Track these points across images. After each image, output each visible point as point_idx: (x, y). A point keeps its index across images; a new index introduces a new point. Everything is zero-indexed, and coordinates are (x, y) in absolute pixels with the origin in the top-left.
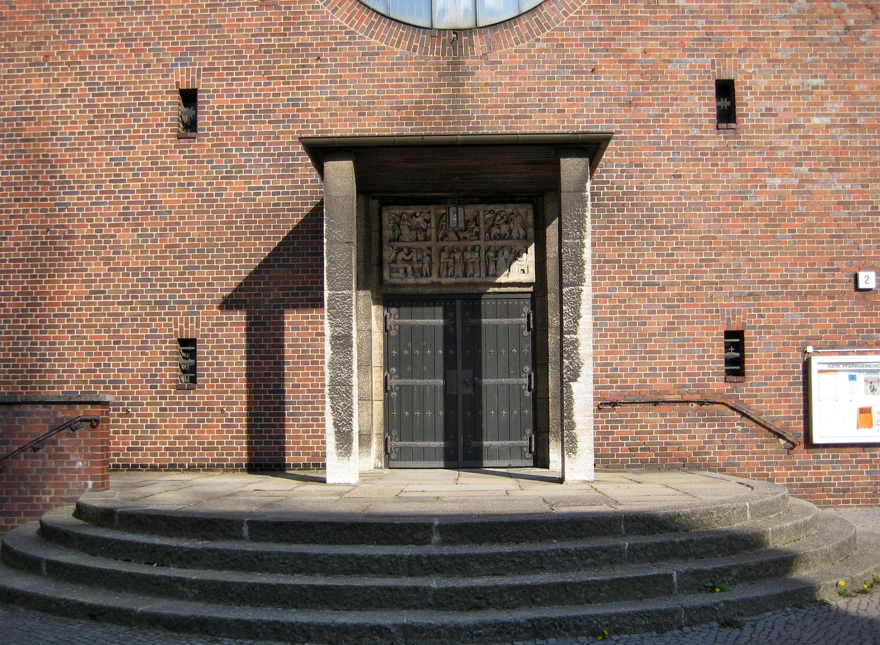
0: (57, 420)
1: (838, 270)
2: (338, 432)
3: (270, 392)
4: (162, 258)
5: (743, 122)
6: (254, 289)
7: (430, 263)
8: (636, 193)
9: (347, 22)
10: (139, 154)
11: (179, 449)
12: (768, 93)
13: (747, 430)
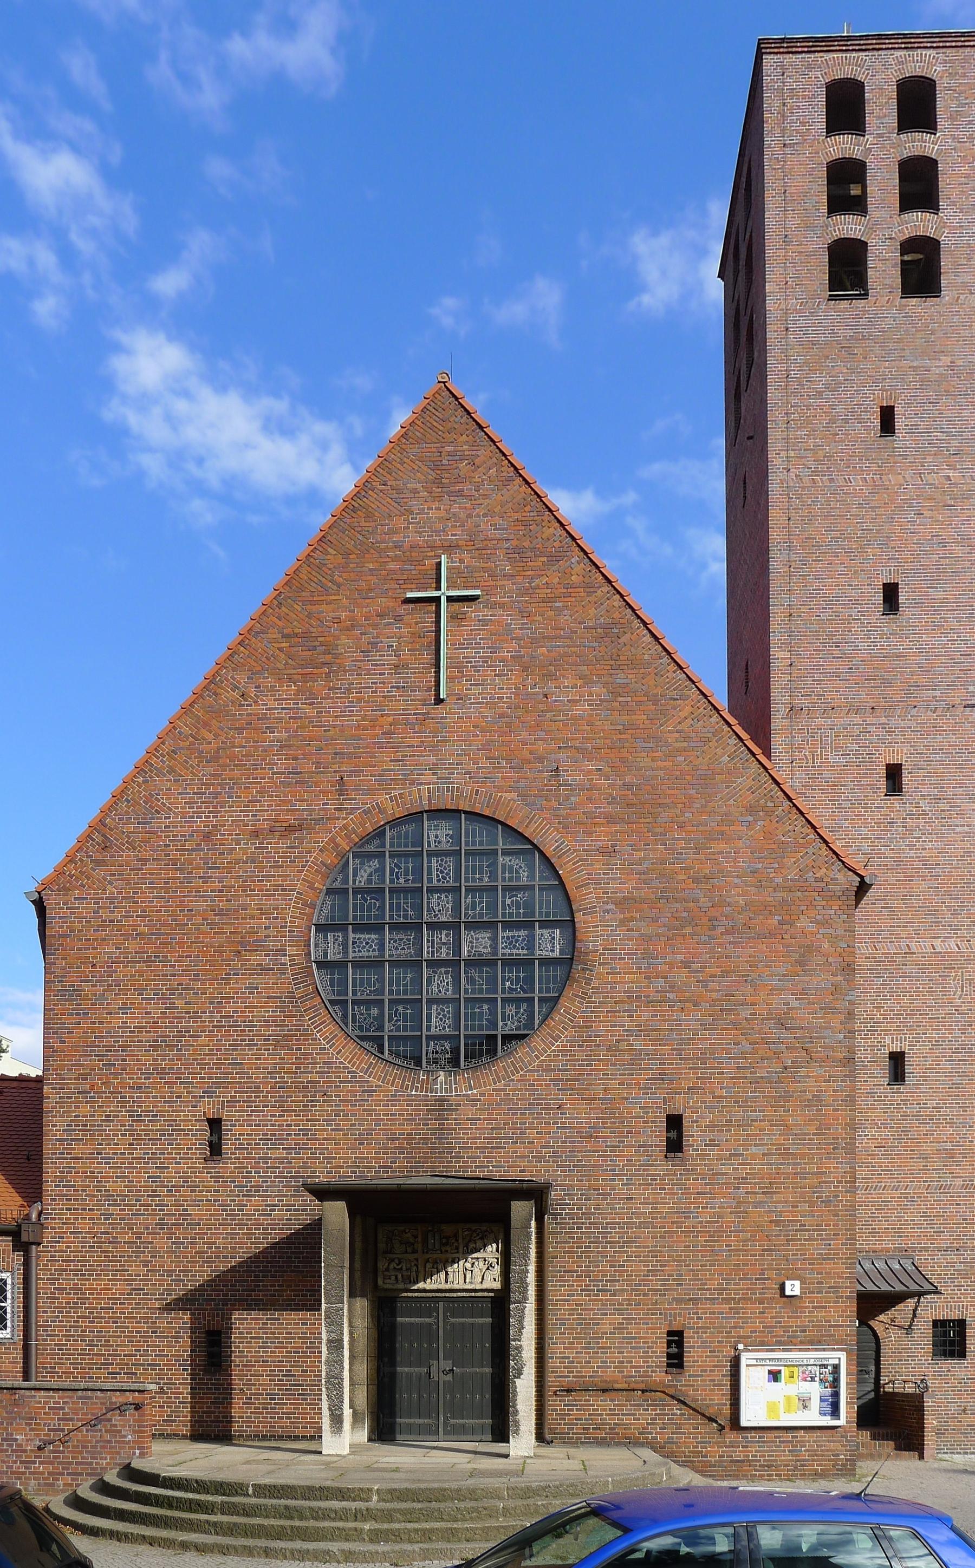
0: (111, 1403)
1: (768, 1279)
2: (332, 1415)
3: (283, 1376)
4: (193, 1262)
5: (689, 1152)
6: (270, 1290)
7: (417, 1272)
8: (594, 1214)
9: (349, 1063)
10: (172, 1174)
11: (206, 1421)
12: (712, 1126)
13: (684, 1414)
